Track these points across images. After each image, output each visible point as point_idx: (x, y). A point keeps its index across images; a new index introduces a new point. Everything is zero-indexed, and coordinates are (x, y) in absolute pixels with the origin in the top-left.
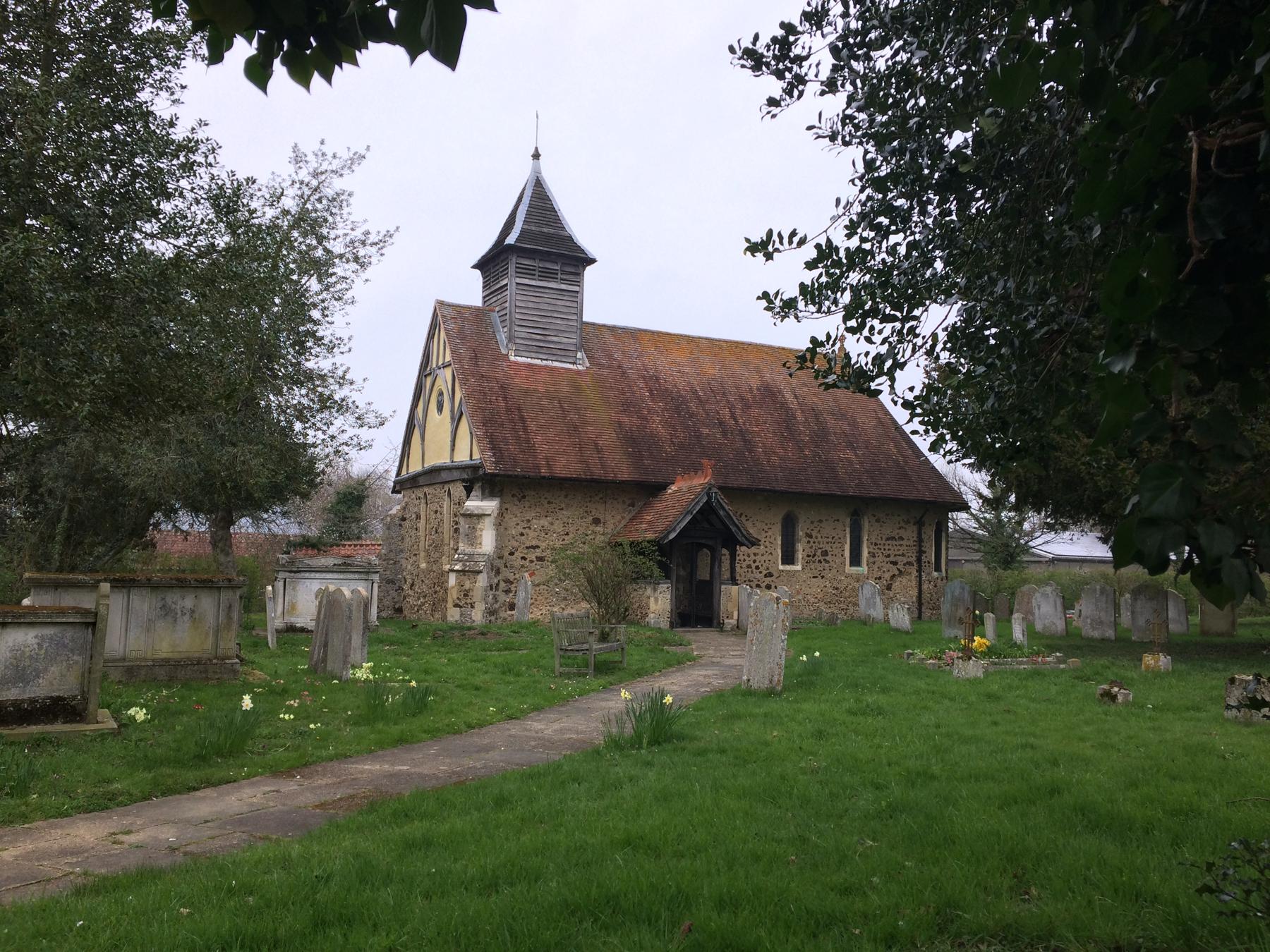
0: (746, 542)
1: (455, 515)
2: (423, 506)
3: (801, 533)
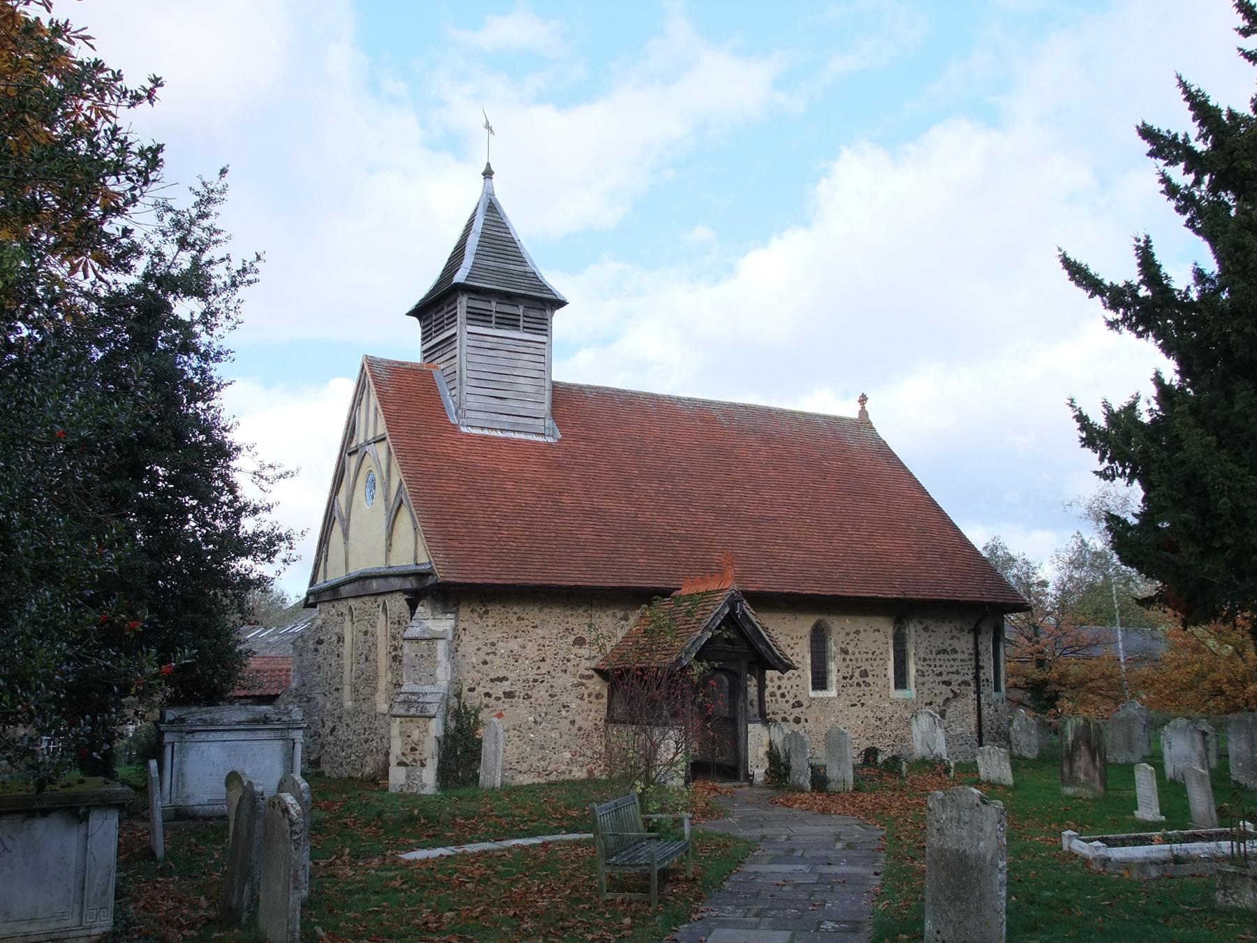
0: (781, 667)
1: (394, 638)
2: (348, 624)
3: (834, 649)
